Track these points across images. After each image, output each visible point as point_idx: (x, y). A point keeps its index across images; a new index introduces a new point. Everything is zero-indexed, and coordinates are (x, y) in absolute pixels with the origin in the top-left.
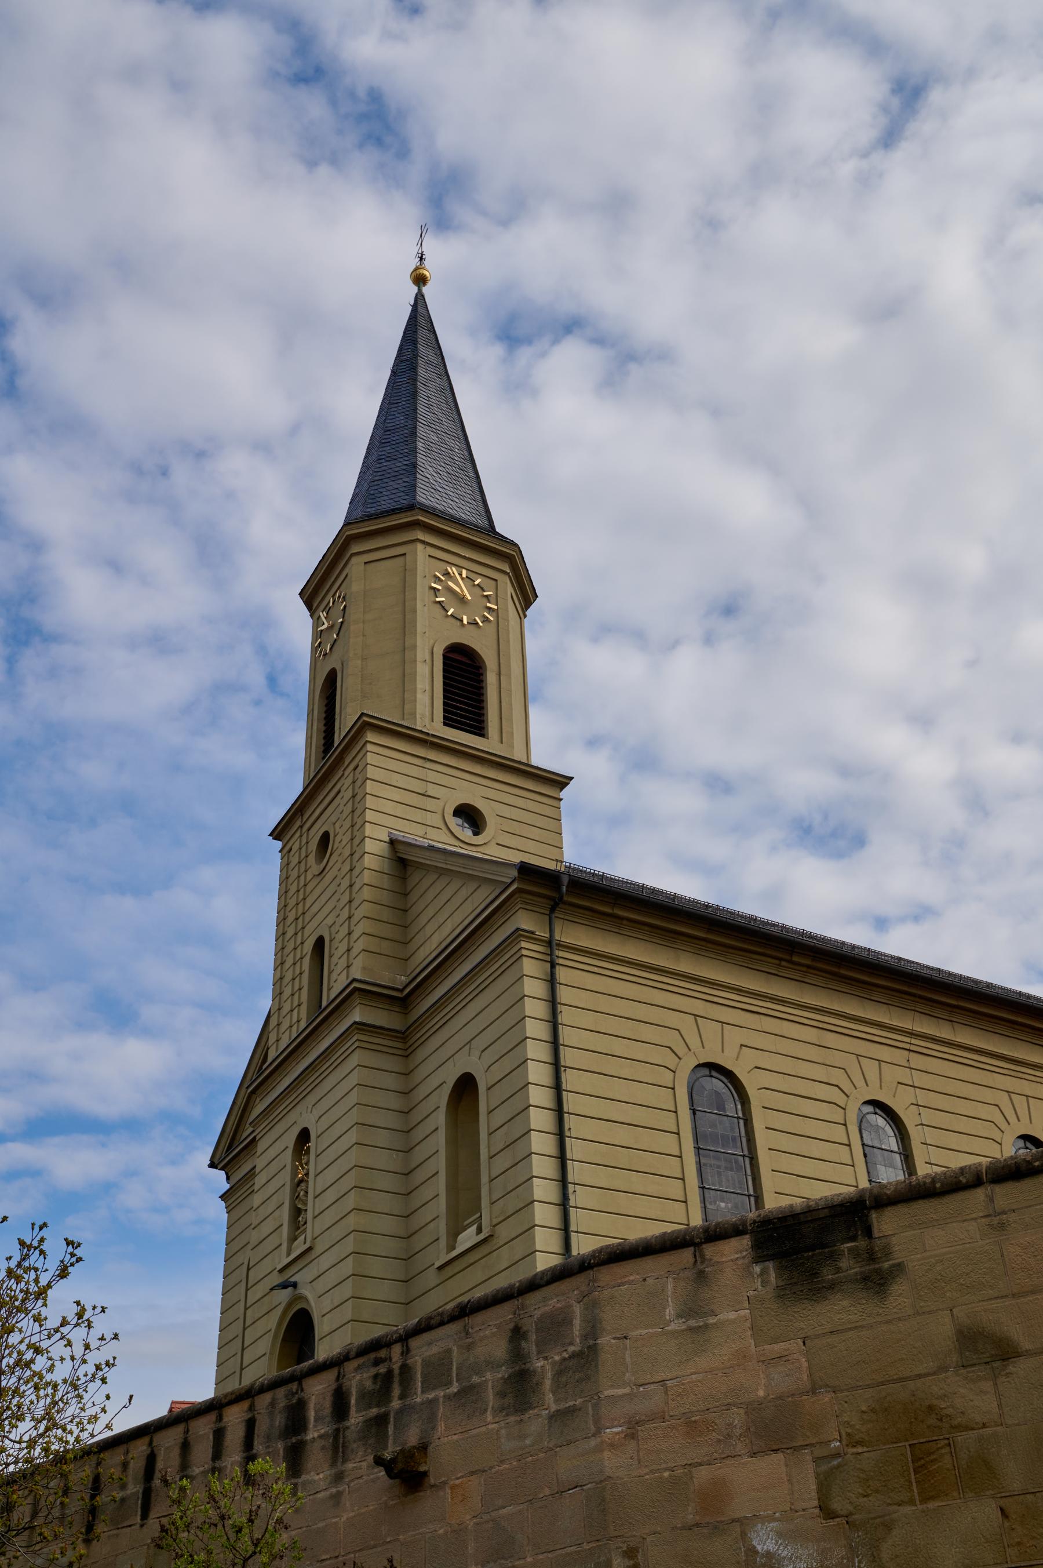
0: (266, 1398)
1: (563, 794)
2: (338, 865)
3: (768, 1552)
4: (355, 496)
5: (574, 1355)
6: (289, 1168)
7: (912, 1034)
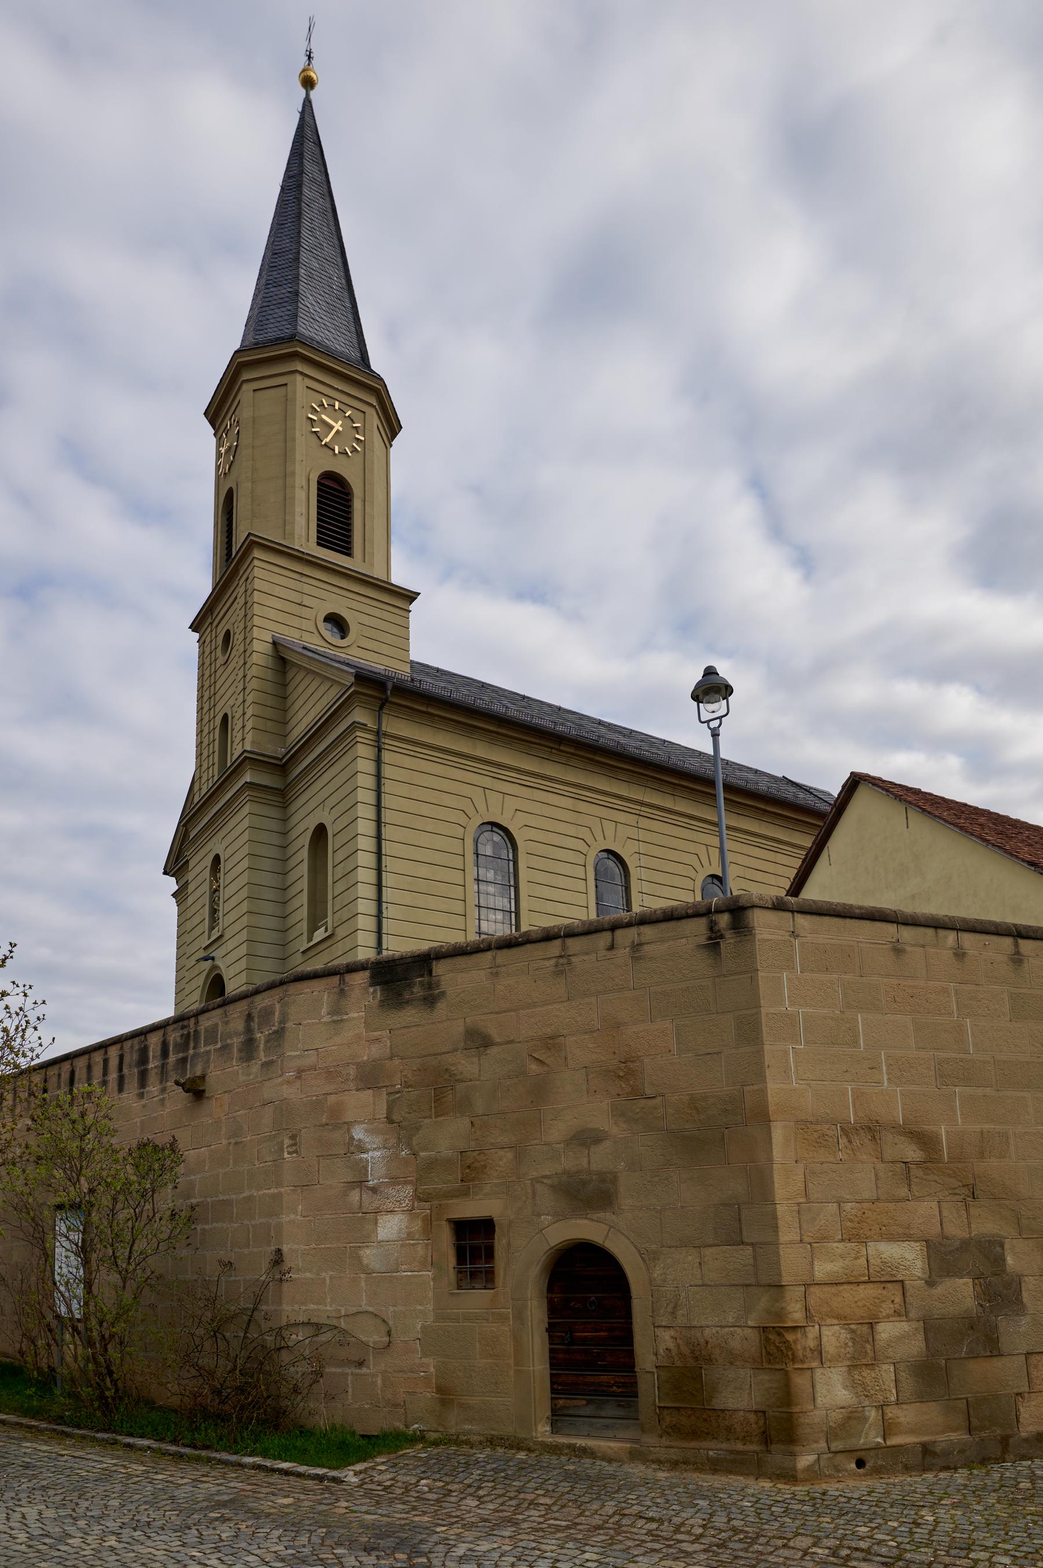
0: (129, 1043)
1: (412, 607)
2: (236, 659)
3: (360, 1139)
4: (249, 318)
5: (275, 1032)
6: (208, 880)
7: (642, 804)
